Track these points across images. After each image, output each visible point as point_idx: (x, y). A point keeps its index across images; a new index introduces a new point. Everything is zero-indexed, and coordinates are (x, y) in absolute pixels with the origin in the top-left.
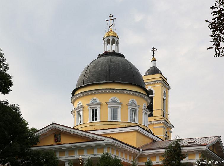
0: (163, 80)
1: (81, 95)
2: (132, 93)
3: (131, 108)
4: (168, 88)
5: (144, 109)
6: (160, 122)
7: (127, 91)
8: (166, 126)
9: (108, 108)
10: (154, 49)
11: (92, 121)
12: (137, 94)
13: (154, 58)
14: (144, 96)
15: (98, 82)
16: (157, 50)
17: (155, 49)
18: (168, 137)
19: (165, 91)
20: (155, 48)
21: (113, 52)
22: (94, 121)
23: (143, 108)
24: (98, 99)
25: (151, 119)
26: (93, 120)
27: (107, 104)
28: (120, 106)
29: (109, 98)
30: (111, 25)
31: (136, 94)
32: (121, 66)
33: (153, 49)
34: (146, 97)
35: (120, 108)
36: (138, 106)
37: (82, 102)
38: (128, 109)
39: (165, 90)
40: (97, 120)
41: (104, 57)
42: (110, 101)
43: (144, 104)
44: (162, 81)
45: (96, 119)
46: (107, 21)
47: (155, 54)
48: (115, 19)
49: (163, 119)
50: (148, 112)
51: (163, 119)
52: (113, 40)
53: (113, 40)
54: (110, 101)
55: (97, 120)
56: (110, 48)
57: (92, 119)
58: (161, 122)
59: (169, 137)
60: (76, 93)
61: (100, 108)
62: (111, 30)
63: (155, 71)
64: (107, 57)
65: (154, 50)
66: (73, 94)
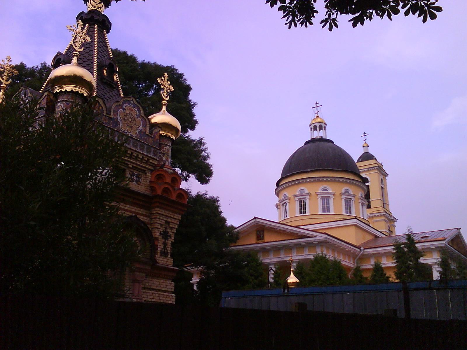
0: (379, 166)
1: (286, 186)
4: (386, 175)
5: (361, 199)
9: (318, 198)
11: (323, 212)
14: (360, 184)
15: (305, 170)
16: (368, 135)
17: (365, 134)
19: (382, 179)
20: (366, 133)
21: (320, 138)
22: (303, 215)
24: (306, 189)
25: (370, 211)
26: (301, 213)
27: (317, 194)
28: (333, 195)
33: (363, 134)
36: (354, 196)
37: (288, 193)
39: (382, 177)
40: (306, 213)
42: (320, 190)
43: (360, 193)
45: (305, 212)
46: (313, 108)
48: (321, 106)
50: (365, 202)
54: (320, 190)
55: (306, 213)
56: (317, 134)
63: (367, 157)
66: (278, 184)
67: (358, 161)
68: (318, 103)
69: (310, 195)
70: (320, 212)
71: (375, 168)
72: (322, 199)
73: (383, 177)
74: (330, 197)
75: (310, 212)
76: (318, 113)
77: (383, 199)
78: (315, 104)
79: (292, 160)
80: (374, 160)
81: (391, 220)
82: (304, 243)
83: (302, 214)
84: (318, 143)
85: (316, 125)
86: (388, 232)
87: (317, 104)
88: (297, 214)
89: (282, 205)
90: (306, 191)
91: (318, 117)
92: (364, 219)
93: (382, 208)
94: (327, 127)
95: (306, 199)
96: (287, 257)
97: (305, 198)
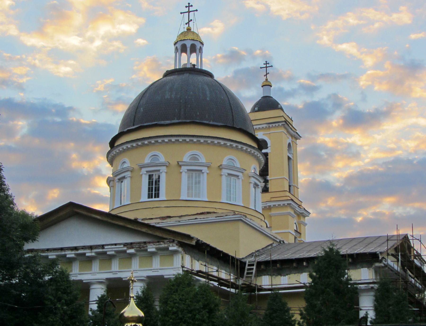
0: (286, 121)
1: (127, 147)
5: (253, 177)
6: (274, 204)
8: (295, 212)
9: (181, 173)
10: (266, 64)
11: (149, 198)
12: (240, 146)
13: (267, 80)
14: (253, 151)
15: (162, 122)
16: (272, 66)
17: (268, 65)
18: (298, 235)
19: (289, 144)
20: (268, 64)
21: (192, 66)
22: (154, 199)
24: (162, 155)
26: (150, 196)
27: (220, 168)
30: (189, 21)
32: (208, 93)
33: (264, 64)
34: (257, 153)
37: (127, 161)
38: (181, 173)
40: (158, 197)
43: (254, 167)
45: (157, 195)
46: (181, 13)
48: (197, 10)
55: (158, 197)
56: (188, 60)
57: (149, 194)
61: (166, 173)
63: (267, 104)
66: (112, 144)
68: (192, 6)
69: (167, 165)
71: (280, 124)
73: (292, 141)
75: (208, 198)
76: (190, 23)
78: (186, 7)
79: (141, 103)
83: (152, 197)
84: (186, 76)
86: (294, 234)
87: (189, 6)
88: (144, 197)
90: (162, 159)
91: (189, 29)
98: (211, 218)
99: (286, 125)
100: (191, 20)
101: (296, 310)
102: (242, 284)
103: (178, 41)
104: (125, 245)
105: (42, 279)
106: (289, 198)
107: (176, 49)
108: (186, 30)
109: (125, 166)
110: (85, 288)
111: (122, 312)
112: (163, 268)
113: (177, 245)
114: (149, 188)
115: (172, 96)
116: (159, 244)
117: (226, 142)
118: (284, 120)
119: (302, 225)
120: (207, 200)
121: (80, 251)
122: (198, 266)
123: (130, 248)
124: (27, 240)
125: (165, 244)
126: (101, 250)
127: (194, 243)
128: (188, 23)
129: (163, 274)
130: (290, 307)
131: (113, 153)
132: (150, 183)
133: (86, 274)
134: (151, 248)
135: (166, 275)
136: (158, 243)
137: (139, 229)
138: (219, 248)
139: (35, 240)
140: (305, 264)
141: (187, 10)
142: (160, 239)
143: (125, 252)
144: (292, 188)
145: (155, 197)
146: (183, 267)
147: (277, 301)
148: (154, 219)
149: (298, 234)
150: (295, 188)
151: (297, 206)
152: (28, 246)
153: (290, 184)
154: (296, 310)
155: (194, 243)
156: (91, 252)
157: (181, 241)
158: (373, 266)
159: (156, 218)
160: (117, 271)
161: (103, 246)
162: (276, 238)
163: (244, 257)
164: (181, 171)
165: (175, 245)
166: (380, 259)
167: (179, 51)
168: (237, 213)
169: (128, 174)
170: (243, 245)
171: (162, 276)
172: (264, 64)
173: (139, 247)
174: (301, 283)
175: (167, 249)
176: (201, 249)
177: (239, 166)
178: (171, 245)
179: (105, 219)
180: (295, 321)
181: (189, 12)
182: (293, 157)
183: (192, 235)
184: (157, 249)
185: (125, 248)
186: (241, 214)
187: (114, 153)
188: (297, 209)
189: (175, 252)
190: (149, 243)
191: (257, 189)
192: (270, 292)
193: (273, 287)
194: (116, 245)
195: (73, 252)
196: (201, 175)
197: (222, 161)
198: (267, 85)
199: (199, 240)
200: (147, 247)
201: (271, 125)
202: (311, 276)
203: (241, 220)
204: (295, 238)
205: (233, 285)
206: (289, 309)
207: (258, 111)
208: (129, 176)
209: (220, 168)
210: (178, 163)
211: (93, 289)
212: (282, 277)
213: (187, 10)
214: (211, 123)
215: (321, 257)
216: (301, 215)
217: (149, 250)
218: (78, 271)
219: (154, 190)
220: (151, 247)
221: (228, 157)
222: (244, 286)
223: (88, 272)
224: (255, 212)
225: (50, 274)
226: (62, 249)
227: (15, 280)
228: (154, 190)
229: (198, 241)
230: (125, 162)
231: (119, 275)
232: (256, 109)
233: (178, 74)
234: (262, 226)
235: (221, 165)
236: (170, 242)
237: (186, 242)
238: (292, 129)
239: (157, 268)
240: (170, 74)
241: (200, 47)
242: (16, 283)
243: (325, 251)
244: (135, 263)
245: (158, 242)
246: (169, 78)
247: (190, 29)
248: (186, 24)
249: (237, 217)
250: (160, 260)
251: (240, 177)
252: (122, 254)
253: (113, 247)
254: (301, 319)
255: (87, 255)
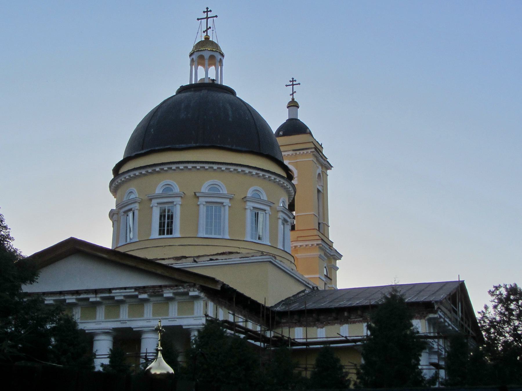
0: (316, 148)
1: (135, 174)
2: (267, 177)
3: (253, 208)
4: (327, 166)
5: (282, 211)
6: (301, 244)
7: (244, 169)
8: (325, 254)
9: (152, 207)
10: (293, 81)
11: (160, 234)
12: (267, 175)
13: (293, 99)
14: (282, 181)
15: (177, 146)
16: (299, 84)
17: (294, 83)
18: (329, 281)
19: (319, 174)
20: (295, 81)
21: (211, 82)
22: (166, 236)
23: (279, 209)
24: (174, 182)
26: (161, 232)
27: (245, 199)
28: (228, 201)
29: (206, 183)
30: (207, 29)
31: (263, 175)
32: (230, 113)
33: (290, 81)
34: (286, 183)
35: (227, 208)
37: (134, 191)
38: (198, 205)
39: (319, 170)
40: (171, 233)
41: (192, 93)
43: (283, 202)
44: (313, 150)
45: (170, 232)
46: (198, 19)
47: (295, 92)
48: (216, 16)
49: (318, 238)
51: (318, 238)
52: (212, 57)
53: (212, 57)
54: (204, 189)
55: (171, 233)
56: (202, 74)
57: (160, 230)
58: (315, 243)
59: (331, 279)
60: (121, 171)
61: (181, 205)
62: (207, 38)
63: (294, 127)
64: (197, 93)
65: (293, 85)
66: (116, 170)
67: (278, 134)
68: (210, 11)
70: (202, 234)
71: (309, 151)
72: (207, 207)
73: (322, 172)
74: (222, 203)
75: (229, 235)
76: (208, 31)
77: (319, 215)
78: (204, 12)
79: (151, 123)
80: (308, 135)
81: (331, 256)
82: (121, 296)
83: (164, 234)
84: (204, 92)
85: (203, 54)
86: (324, 279)
87: (207, 12)
88: (155, 234)
89: (122, 214)
90: (177, 189)
91: (207, 38)
92: (284, 251)
93: (316, 232)
94: (224, 61)
95: (175, 205)
96: (182, 318)
97: (173, 202)
98: (235, 259)
99: (316, 153)
100: (210, 28)
101: (351, 369)
102: (274, 337)
103: (194, 52)
104: (137, 289)
105: (43, 327)
106: (319, 238)
107: (192, 61)
108: (203, 39)
109: (132, 196)
110: (89, 338)
111: (148, 368)
112: (132, 319)
113: (198, 289)
114: (160, 223)
115: (189, 115)
116: (177, 289)
117: (251, 170)
118: (313, 146)
119: (333, 270)
120: (229, 238)
121: (82, 296)
122: (223, 314)
123: (143, 293)
124: (24, 280)
125: (184, 288)
126: (108, 295)
127: (219, 288)
128: (207, 31)
129: (182, 324)
130: (343, 364)
131: (117, 182)
132: (162, 216)
133: (182, 318)
134: (168, 294)
135: (185, 325)
136: (175, 288)
137: (154, 270)
138: (247, 294)
139: (34, 281)
140: (346, 314)
141: (205, 16)
142: (181, 283)
143: (136, 296)
144: (321, 225)
145: (168, 234)
146: (207, 316)
147: (328, 356)
148: (166, 259)
149: (329, 280)
150: (325, 226)
151: (327, 247)
152: (26, 288)
153: (320, 222)
154: (351, 369)
155: (219, 288)
156: (96, 297)
157: (204, 285)
158: (427, 318)
159: (169, 259)
160: (125, 319)
161: (110, 290)
162: (308, 284)
163: (273, 305)
164: (199, 203)
165: (196, 290)
166: (436, 309)
167: (196, 63)
168: (265, 254)
169: (136, 206)
170: (272, 291)
171: (181, 326)
172: (290, 81)
173: (153, 292)
174: (343, 337)
175: (187, 294)
176: (225, 295)
177: (265, 198)
178: (191, 289)
179: (113, 258)
180: (349, 381)
181: (207, 18)
182: (323, 190)
183: (218, 278)
184: (175, 294)
185: (137, 293)
186: (270, 255)
187: (119, 181)
188: (327, 251)
189: (197, 298)
190: (166, 286)
191: (286, 226)
192: (305, 347)
193: (309, 340)
194: (125, 288)
195: (74, 297)
196: (222, 209)
197: (247, 192)
198: (293, 105)
199: (225, 284)
200: (162, 291)
201: (298, 152)
202: (369, 327)
203: (270, 262)
204: (325, 284)
205: (264, 339)
206: (342, 367)
207: (284, 135)
208: (137, 208)
209: (245, 199)
210: (195, 194)
211: (98, 340)
212: (319, 330)
213: (205, 16)
214: (234, 147)
215: (381, 305)
216: (332, 257)
217: (165, 295)
218: (176, 315)
219: (166, 225)
220: (168, 292)
221: (254, 188)
222: (275, 339)
223: (110, 320)
224: (285, 253)
225: (53, 321)
226: (61, 293)
227: (10, 329)
228: (166, 225)
229: (224, 285)
230: (131, 192)
231: (128, 325)
232: (281, 133)
233: (195, 91)
234: (292, 269)
235: (245, 197)
236: (191, 286)
237: (210, 286)
238: (322, 158)
239: (173, 316)
240: (184, 90)
241: (221, 59)
242: (12, 332)
243: (386, 298)
244: (148, 310)
245: (176, 286)
246: (184, 95)
247: (209, 39)
248: (204, 32)
249: (265, 258)
250: (178, 309)
251: (267, 212)
252: (132, 300)
253: (122, 291)
254: (358, 378)
255: (91, 300)
